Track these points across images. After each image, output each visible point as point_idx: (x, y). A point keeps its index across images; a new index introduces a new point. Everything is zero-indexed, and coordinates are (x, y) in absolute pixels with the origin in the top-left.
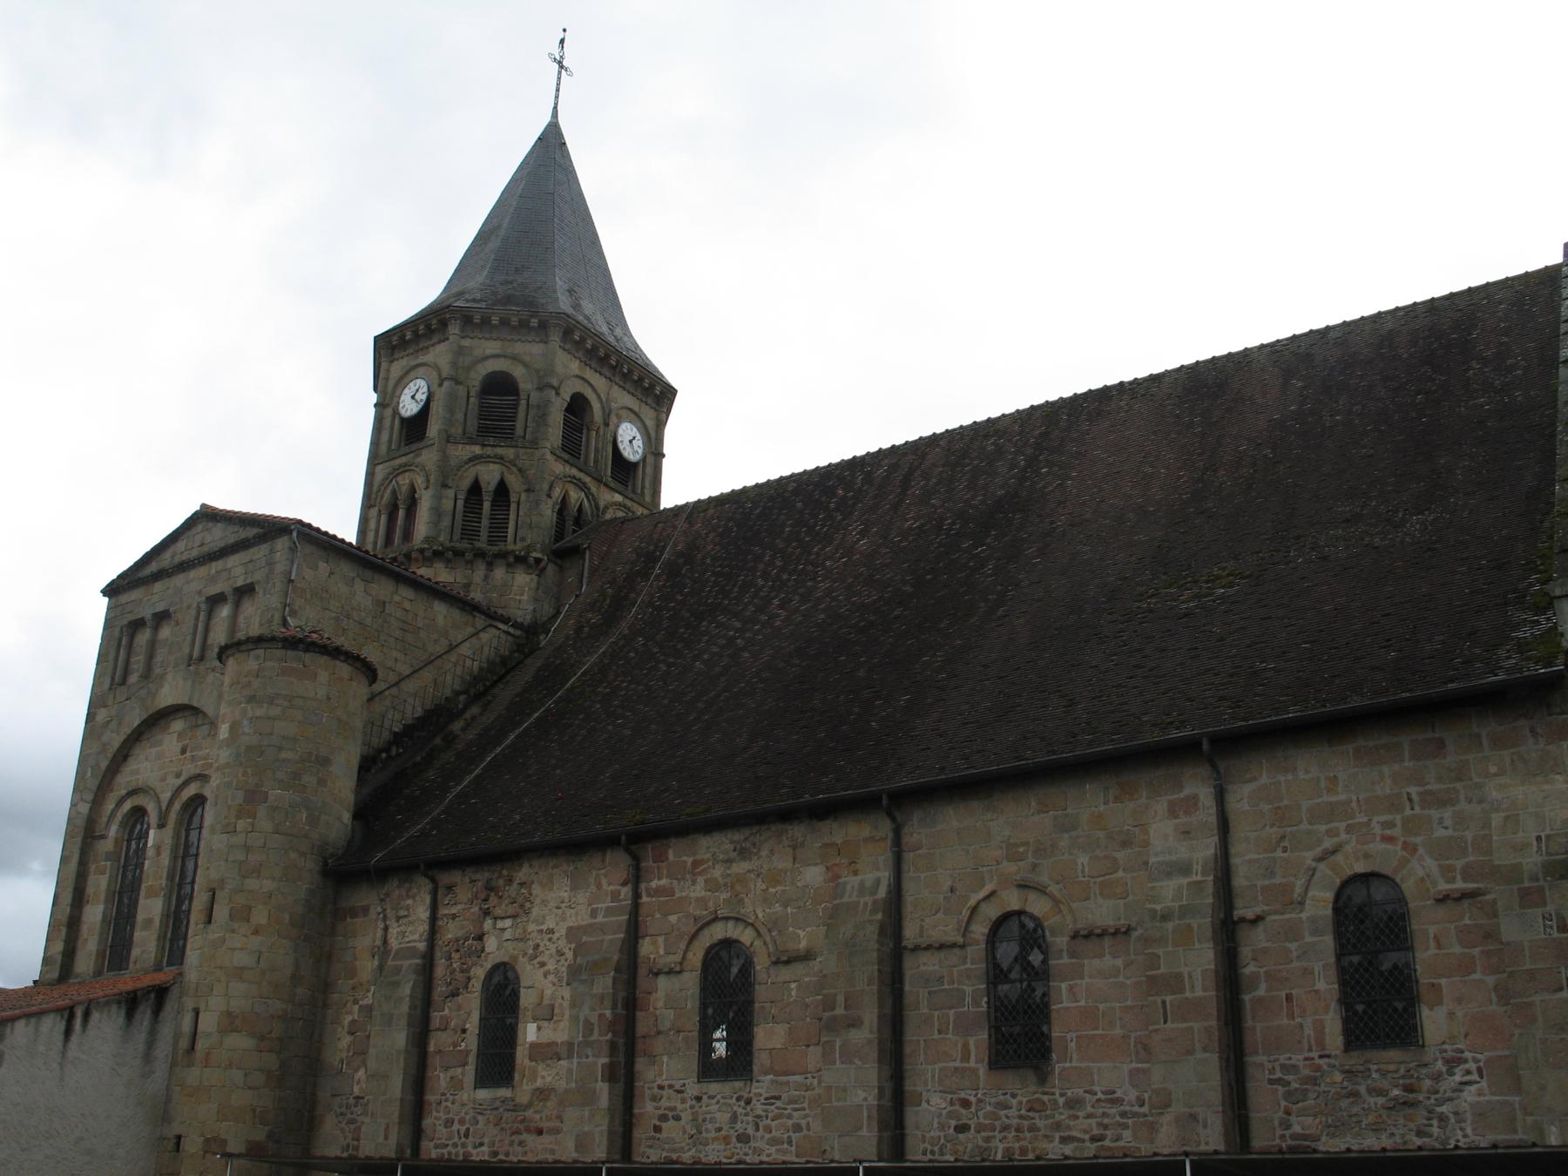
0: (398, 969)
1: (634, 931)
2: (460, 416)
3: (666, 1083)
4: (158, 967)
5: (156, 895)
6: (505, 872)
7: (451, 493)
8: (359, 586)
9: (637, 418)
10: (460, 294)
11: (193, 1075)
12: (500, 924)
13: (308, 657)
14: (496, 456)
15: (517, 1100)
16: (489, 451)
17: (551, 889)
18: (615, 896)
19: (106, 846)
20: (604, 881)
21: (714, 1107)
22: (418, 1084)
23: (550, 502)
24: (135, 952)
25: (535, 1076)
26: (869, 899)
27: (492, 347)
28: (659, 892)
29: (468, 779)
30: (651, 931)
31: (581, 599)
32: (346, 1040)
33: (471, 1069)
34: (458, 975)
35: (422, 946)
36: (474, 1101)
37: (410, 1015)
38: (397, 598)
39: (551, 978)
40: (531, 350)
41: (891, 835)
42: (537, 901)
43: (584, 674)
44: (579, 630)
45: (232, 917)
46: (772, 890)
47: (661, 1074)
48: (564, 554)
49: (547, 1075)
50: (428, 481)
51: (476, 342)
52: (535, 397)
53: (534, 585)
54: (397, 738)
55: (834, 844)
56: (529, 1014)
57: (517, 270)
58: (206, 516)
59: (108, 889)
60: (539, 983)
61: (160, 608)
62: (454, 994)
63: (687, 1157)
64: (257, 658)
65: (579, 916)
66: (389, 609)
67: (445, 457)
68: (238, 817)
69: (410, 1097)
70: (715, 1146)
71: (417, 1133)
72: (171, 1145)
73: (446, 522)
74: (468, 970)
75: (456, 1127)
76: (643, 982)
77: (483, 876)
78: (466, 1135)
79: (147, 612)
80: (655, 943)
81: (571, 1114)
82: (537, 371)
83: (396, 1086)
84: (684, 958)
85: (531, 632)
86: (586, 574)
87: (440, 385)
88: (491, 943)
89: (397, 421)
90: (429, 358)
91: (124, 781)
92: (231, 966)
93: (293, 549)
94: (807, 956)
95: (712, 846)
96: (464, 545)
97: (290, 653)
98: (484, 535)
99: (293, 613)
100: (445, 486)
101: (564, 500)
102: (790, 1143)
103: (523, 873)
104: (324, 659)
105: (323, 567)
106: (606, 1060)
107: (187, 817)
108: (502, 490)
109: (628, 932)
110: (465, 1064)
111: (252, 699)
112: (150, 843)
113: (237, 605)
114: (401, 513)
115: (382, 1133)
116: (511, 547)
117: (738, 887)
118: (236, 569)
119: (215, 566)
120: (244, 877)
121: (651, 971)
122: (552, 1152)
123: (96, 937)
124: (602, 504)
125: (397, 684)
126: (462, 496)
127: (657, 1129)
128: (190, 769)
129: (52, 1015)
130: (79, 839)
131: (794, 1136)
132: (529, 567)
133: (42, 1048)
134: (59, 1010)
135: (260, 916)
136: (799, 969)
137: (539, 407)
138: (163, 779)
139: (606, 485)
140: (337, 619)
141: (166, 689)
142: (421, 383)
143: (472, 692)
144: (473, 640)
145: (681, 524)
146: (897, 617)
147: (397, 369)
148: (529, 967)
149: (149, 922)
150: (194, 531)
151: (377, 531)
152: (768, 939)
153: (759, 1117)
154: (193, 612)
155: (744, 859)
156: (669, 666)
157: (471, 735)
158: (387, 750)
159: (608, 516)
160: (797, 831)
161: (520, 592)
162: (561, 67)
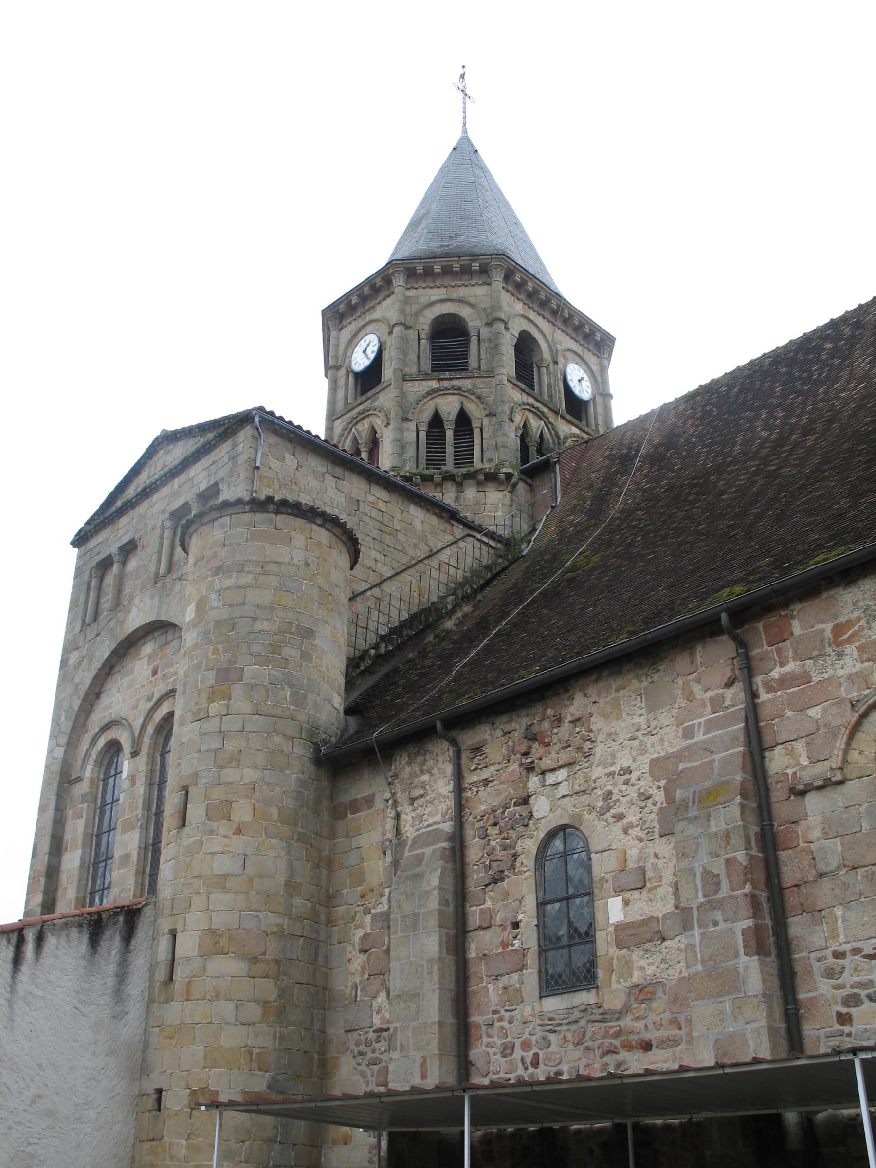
0: (420, 859)
1: (757, 743)
2: (413, 357)
3: (847, 947)
5: (133, 828)
6: (550, 712)
7: (412, 426)
8: (330, 481)
12: (550, 778)
13: (281, 520)
14: (453, 388)
15: (606, 1006)
16: (446, 384)
17: (619, 717)
18: (717, 704)
19: (83, 787)
20: (697, 689)
22: (460, 1001)
23: (513, 427)
25: (625, 970)
27: (437, 294)
28: (784, 682)
31: (557, 510)
33: (531, 975)
34: (500, 854)
35: (447, 827)
36: (541, 1015)
37: (440, 912)
38: (371, 498)
39: (633, 832)
40: (477, 292)
42: (600, 738)
47: (835, 935)
49: (645, 965)
50: (388, 419)
51: (421, 291)
52: (485, 332)
53: (507, 501)
56: (608, 886)
57: (450, 237)
58: (168, 439)
59: (85, 834)
60: (613, 844)
61: (126, 539)
62: (496, 880)
64: (223, 526)
65: (669, 740)
67: (403, 395)
68: (211, 700)
69: (450, 1020)
71: (465, 1066)
72: (151, 1102)
73: (411, 452)
74: (513, 846)
75: (518, 1053)
77: (519, 724)
80: (791, 753)
81: (702, 1011)
82: (484, 309)
83: (432, 1005)
84: (845, 761)
86: (559, 487)
87: (391, 333)
88: (541, 806)
89: (351, 379)
90: (376, 315)
92: (217, 873)
93: (256, 438)
97: (259, 516)
100: (406, 420)
103: (577, 705)
104: (299, 522)
105: (291, 461)
106: (749, 923)
107: (161, 740)
108: (463, 420)
109: (748, 743)
110: (523, 967)
111: (219, 570)
119: (177, 482)
120: (222, 767)
123: (75, 884)
124: (562, 435)
125: (378, 585)
126: (424, 428)
127: (844, 1019)
128: (162, 688)
130: (55, 786)
132: (501, 483)
135: (242, 812)
137: (490, 340)
138: (135, 707)
139: (562, 417)
143: (460, 593)
144: (454, 548)
148: (600, 825)
149: (126, 857)
151: (347, 385)
154: (158, 532)
161: (494, 507)
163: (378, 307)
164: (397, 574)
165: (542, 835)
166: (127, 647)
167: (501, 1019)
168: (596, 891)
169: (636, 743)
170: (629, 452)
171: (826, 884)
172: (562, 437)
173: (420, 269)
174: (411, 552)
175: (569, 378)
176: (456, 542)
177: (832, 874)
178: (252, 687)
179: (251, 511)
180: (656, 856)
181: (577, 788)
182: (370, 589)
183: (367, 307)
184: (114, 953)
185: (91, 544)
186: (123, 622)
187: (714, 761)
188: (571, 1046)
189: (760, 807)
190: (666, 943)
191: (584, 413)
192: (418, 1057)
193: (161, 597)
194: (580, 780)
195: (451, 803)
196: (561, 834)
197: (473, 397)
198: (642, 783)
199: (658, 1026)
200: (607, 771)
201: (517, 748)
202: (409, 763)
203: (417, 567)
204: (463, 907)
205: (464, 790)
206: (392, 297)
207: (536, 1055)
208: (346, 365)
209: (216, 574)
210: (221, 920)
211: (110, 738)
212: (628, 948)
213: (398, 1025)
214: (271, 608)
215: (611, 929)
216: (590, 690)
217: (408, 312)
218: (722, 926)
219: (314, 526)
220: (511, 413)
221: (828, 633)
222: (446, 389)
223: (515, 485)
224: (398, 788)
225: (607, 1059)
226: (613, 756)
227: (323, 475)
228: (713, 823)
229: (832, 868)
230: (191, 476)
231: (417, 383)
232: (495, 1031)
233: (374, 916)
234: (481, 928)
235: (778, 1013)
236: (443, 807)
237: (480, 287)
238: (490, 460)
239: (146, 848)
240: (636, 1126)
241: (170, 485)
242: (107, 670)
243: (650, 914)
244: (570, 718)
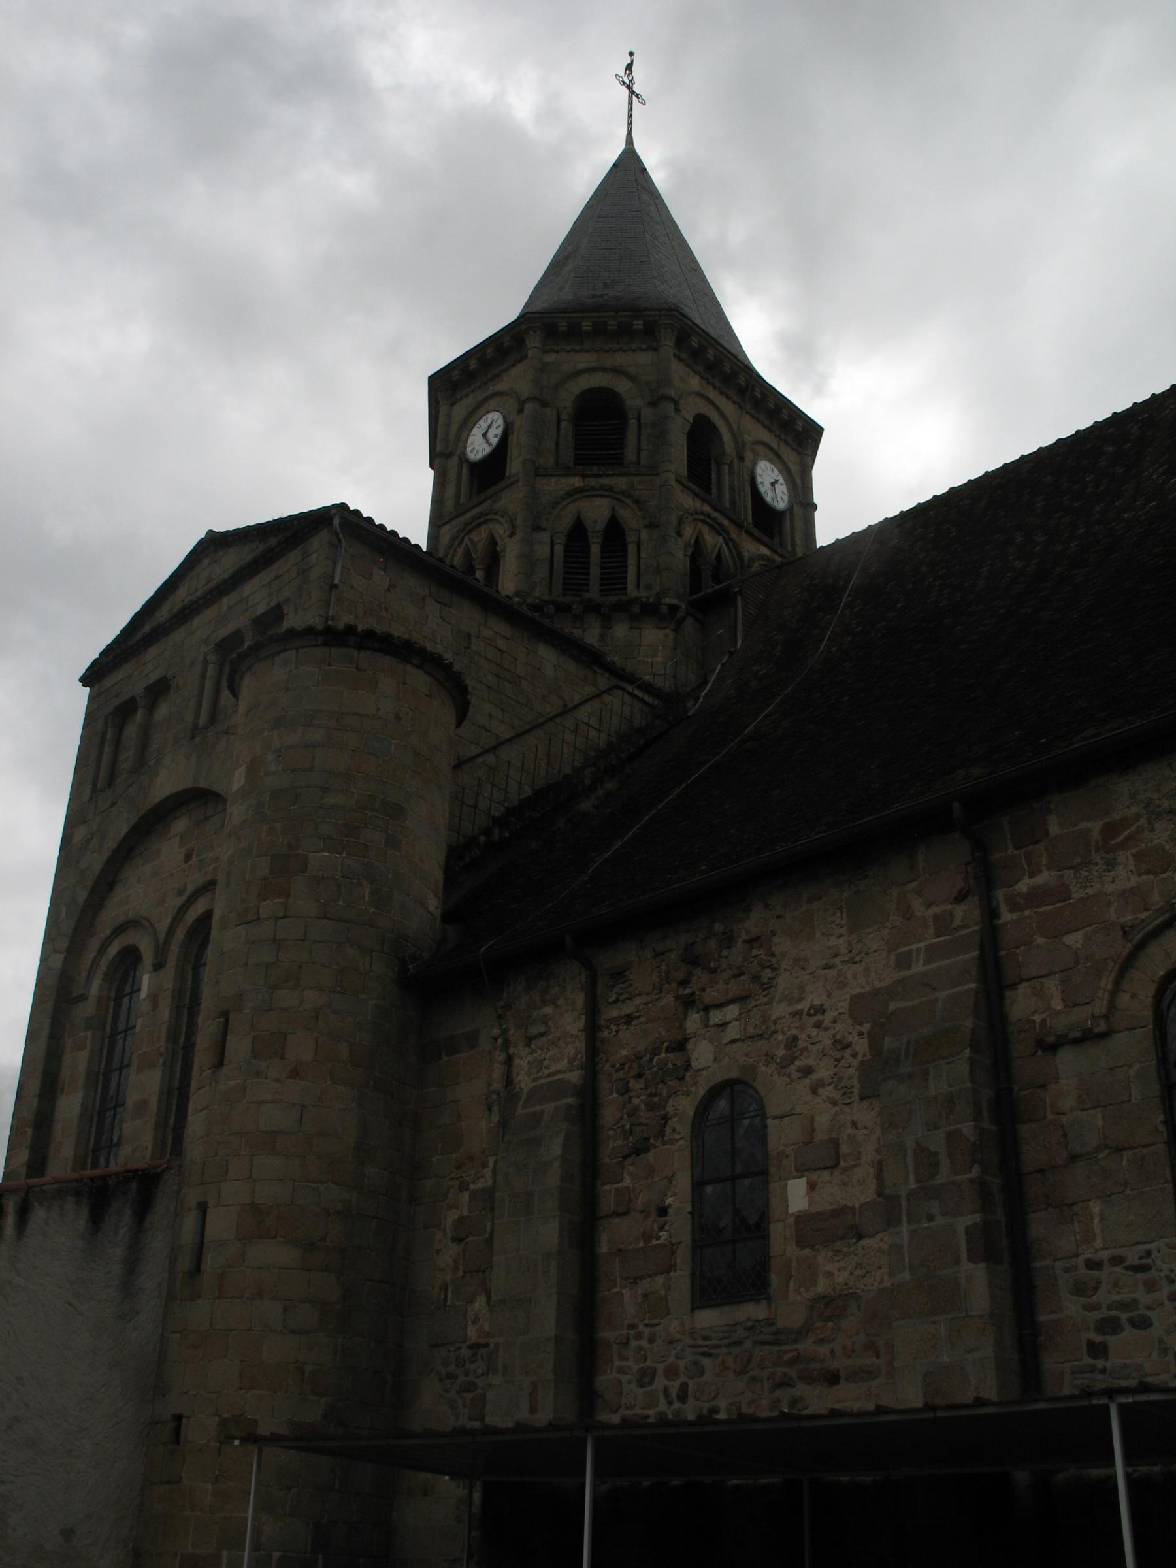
1: (994, 977)
3: (1105, 1255)
6: (718, 927)
7: (545, 537)
9: (777, 458)
12: (716, 1017)
14: (602, 487)
16: (593, 482)
18: (942, 924)
19: (88, 1009)
20: (917, 904)
27: (584, 360)
28: (1035, 897)
32: (449, 1253)
33: (681, 1279)
35: (575, 1077)
38: (487, 633)
39: (827, 1092)
40: (639, 360)
49: (834, 1271)
50: (513, 526)
52: (648, 414)
57: (606, 285)
58: (214, 544)
60: (797, 1107)
62: (639, 1150)
71: (587, 1395)
73: (542, 573)
75: (660, 1382)
79: (137, 690)
83: (547, 1315)
84: (1112, 1006)
86: (740, 627)
87: (521, 411)
88: (702, 1053)
90: (502, 386)
91: (111, 915)
100: (537, 528)
101: (698, 543)
103: (753, 922)
105: (380, 579)
106: (977, 1218)
108: (614, 532)
110: (671, 1268)
118: (257, 595)
119: (226, 602)
124: (746, 555)
125: (493, 749)
126: (560, 541)
127: (1098, 1350)
128: (197, 879)
139: (748, 533)
147: (460, 411)
164: (517, 736)
165: (702, 1092)
167: (639, 1336)
169: (832, 973)
173: (563, 326)
175: (759, 479)
179: (326, 644)
180: (854, 1125)
181: (751, 1031)
184: (122, 1231)
185: (108, 682)
190: (864, 1242)
195: (581, 1045)
197: (628, 501)
198: (838, 1027)
200: (791, 1009)
207: (684, 1386)
212: (813, 1247)
215: (791, 1220)
218: (939, 1221)
219: (409, 668)
221: (1096, 834)
222: (593, 489)
225: (777, 1393)
226: (802, 989)
227: (423, 599)
230: (245, 595)
231: (553, 479)
236: (570, 1050)
244: (744, 936)
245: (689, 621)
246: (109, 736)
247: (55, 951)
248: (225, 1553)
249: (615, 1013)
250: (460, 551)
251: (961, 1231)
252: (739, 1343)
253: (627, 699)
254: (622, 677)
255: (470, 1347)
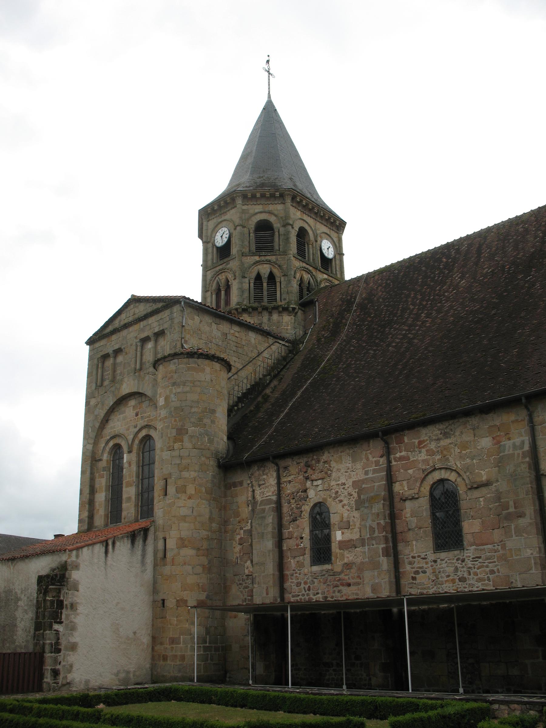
1: (390, 480)
2: (246, 243)
3: (416, 555)
4: (136, 520)
5: (131, 486)
6: (315, 457)
7: (247, 280)
8: (214, 326)
10: (238, 185)
11: (167, 570)
12: (315, 483)
14: (266, 260)
15: (335, 570)
16: (263, 258)
17: (341, 463)
18: (377, 463)
19: (103, 464)
20: (370, 456)
21: (444, 565)
22: (281, 566)
23: (295, 280)
24: (124, 514)
25: (341, 558)
26: (520, 452)
27: (258, 208)
28: (401, 459)
29: (282, 415)
30: (399, 479)
31: (317, 326)
32: (238, 548)
33: (307, 558)
34: (295, 510)
35: (274, 498)
36: (311, 573)
37: (273, 532)
38: (232, 331)
39: (346, 507)
40: (278, 208)
41: (527, 418)
43: (328, 360)
44: (319, 340)
45: (177, 492)
46: (463, 452)
47: (412, 550)
48: (306, 305)
49: (349, 556)
50: (235, 276)
51: (250, 207)
52: (282, 230)
53: (293, 321)
54: (240, 400)
55: (495, 426)
56: (336, 527)
57: (264, 171)
58: (135, 300)
59: (106, 486)
60: (338, 511)
61: (116, 347)
62: (295, 520)
63: (431, 591)
64: (175, 363)
65: (359, 475)
66: (229, 337)
69: (277, 573)
70: (447, 584)
71: (282, 591)
73: (246, 294)
74: (300, 508)
75: (303, 586)
76: (398, 505)
77: (303, 460)
78: (309, 590)
79: (110, 350)
80: (401, 485)
81: (367, 574)
82: (282, 218)
83: (271, 568)
84: (419, 490)
85: (294, 345)
86: (317, 313)
87: (235, 229)
88: (311, 493)
89: (215, 249)
90: (227, 217)
91: (108, 431)
93: (182, 311)
94: (487, 484)
95: (426, 433)
96: (256, 305)
98: (265, 299)
99: (186, 342)
100: (244, 277)
101: (301, 279)
102: (489, 580)
103: (325, 456)
104: (207, 362)
106: (384, 545)
107: (142, 446)
108: (271, 277)
110: (304, 554)
111: (174, 384)
112: (125, 460)
113: (156, 341)
114: (223, 293)
115: (265, 590)
116: (280, 304)
117: (445, 453)
118: (154, 324)
119: (142, 324)
120: (181, 471)
121: (401, 499)
122: (357, 594)
124: (319, 280)
125: (236, 373)
126: (252, 282)
127: (414, 578)
128: (141, 423)
129: (98, 545)
131: (491, 576)
132: (290, 312)
133: (96, 561)
134: (101, 542)
135: (191, 490)
136: (484, 490)
137: (284, 235)
138: (128, 429)
139: (320, 271)
140: (206, 343)
141: (124, 386)
142: (225, 229)
143: (272, 374)
144: (269, 350)
145: (362, 285)
146: (495, 314)
149: (129, 499)
150: (129, 309)
151: (213, 252)
152: (465, 477)
153: (470, 568)
154: (134, 347)
155: (447, 438)
156: (375, 351)
157: (277, 395)
158: (237, 405)
159: (322, 285)
160: (474, 421)
161: (288, 325)
162: (270, 74)
163: (228, 213)
165: (312, 505)
166: (122, 401)
167: (296, 573)
168: (332, 528)
169: (347, 474)
170: (351, 299)
171: (411, 533)
172: (319, 281)
173: (249, 195)
174: (250, 355)
175: (323, 248)
176: (270, 346)
177: (412, 530)
178: (192, 437)
179: (187, 357)
180: (354, 517)
181: (325, 488)
182: (233, 375)
183: (222, 212)
185: (97, 345)
186: (120, 388)
187: (374, 486)
188: (322, 584)
189: (390, 504)
190: (357, 549)
191: (330, 267)
192: (265, 586)
193: (138, 381)
194: (326, 485)
195: (276, 488)
196: (319, 505)
197: (276, 266)
198: (349, 489)
199: (353, 578)
200: (336, 483)
201: (302, 470)
202: (258, 470)
203: (253, 362)
204: (281, 530)
205: (281, 484)
206: (235, 208)
207: (309, 587)
208: (212, 241)
209: (173, 386)
210: (185, 534)
211: (115, 442)
212: (343, 550)
213: (256, 575)
214: (198, 402)
215: (337, 542)
216: (330, 451)
217: (244, 218)
218: (375, 546)
219: (214, 363)
220: (295, 274)
221: (416, 443)
223: (297, 313)
224: (253, 480)
225: (335, 589)
226: (339, 477)
228: (373, 509)
229: (413, 527)
230: (150, 323)
231: (249, 257)
232: (294, 578)
233: (244, 531)
234: (288, 538)
235: (393, 576)
236: (272, 489)
237: (280, 205)
238: (285, 299)
239: (138, 495)
240: (344, 612)
241: (138, 324)
242: (111, 410)
243: (351, 538)
244: (323, 461)
245: (300, 312)
246: (100, 366)
247: (88, 443)
248: (182, 637)
249: (286, 480)
250: (216, 281)
251: (381, 549)
252: (324, 575)
253: (280, 345)
254: (277, 337)
255: (246, 576)
